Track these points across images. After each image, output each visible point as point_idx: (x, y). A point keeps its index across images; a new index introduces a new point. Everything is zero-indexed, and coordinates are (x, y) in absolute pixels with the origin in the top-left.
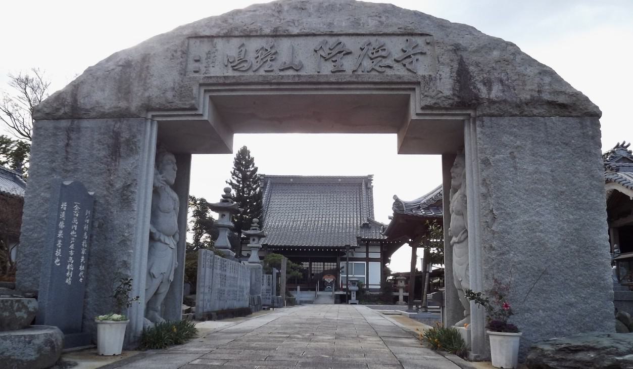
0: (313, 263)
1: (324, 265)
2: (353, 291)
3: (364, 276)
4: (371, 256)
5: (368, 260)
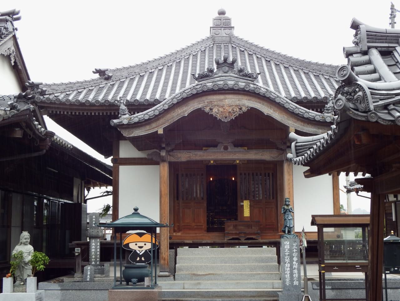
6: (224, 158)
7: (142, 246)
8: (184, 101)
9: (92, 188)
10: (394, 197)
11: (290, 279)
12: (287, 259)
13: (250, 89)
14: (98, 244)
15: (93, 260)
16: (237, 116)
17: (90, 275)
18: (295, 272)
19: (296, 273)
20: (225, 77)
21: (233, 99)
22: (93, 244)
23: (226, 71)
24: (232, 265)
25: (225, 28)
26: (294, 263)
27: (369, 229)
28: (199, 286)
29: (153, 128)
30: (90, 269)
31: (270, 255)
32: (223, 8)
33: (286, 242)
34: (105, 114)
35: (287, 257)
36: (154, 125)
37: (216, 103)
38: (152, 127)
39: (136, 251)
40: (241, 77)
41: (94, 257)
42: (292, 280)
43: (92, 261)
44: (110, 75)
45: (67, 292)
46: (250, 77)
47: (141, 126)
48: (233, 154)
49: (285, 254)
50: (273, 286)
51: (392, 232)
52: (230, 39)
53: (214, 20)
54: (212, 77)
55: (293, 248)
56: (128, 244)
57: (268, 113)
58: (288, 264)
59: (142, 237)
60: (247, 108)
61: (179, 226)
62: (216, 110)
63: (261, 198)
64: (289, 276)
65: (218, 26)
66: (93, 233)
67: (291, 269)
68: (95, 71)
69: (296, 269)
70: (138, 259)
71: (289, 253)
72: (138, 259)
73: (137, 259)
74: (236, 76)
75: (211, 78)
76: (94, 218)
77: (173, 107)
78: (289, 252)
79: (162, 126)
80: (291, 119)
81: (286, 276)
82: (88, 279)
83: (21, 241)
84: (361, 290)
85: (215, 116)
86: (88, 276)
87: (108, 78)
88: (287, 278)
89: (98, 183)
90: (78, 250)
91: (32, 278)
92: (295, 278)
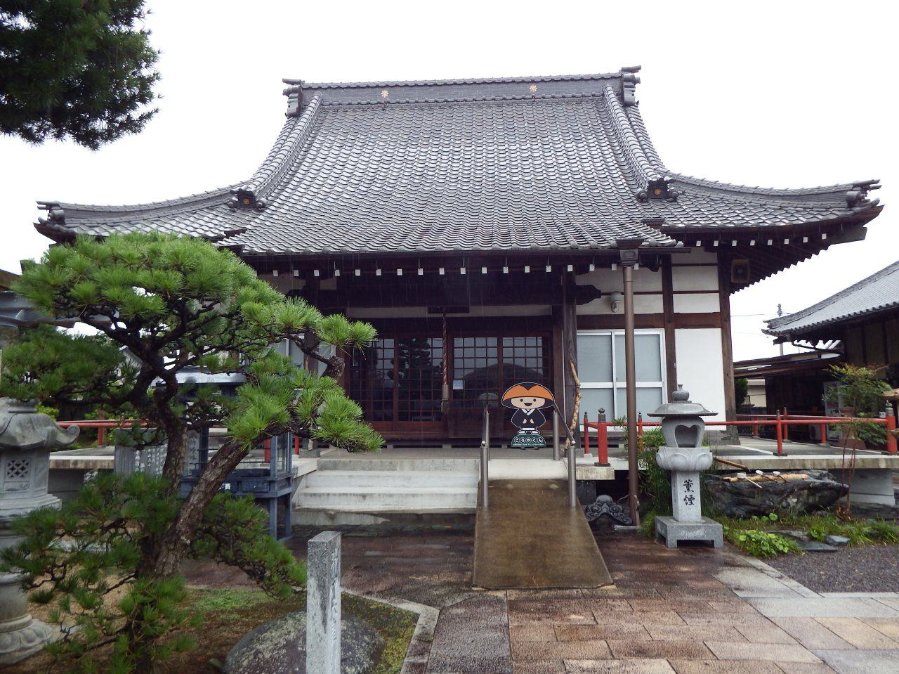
0: (458, 342)
1: (500, 346)
2: (687, 472)
3: (659, 384)
4: (683, 305)
5: (672, 321)
61: (264, 345)
63: (746, 261)
70: (525, 421)
72: (525, 421)
84: (471, 349)
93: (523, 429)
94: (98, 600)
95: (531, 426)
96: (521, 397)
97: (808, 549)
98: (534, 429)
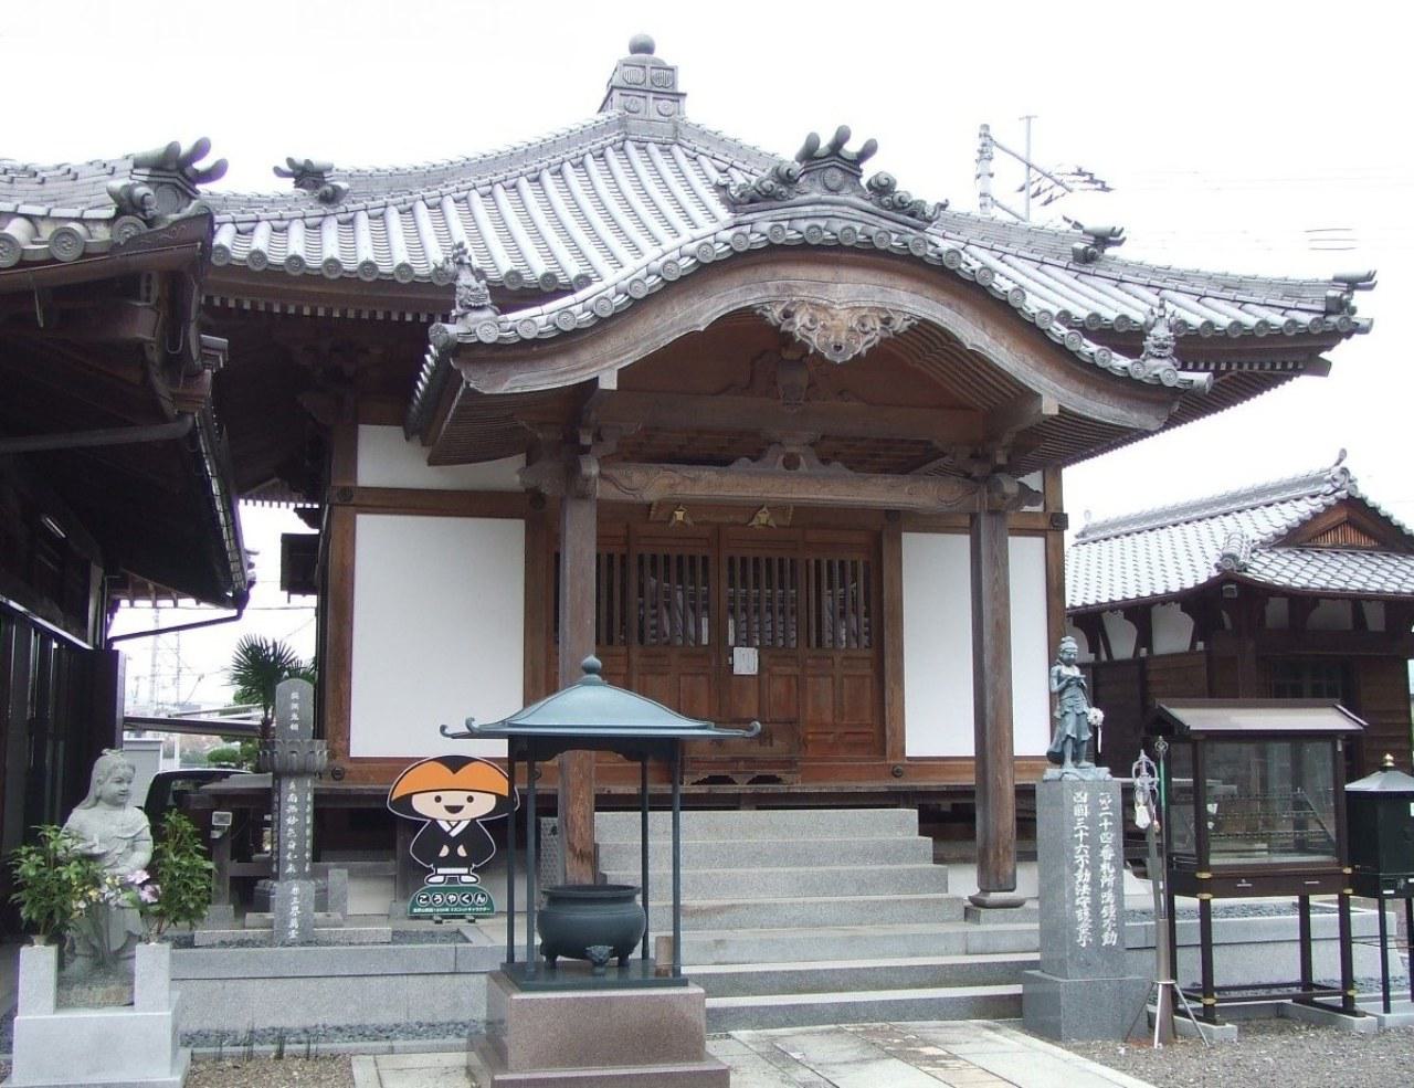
6: (789, 495)
7: (460, 804)
8: (674, 287)
9: (124, 603)
10: (1090, 652)
11: (1091, 924)
12: (1082, 853)
13: (926, 255)
14: (309, 798)
15: (289, 857)
16: (874, 346)
17: (298, 916)
18: (1108, 900)
19: (1108, 904)
20: (828, 207)
21: (863, 286)
22: (293, 798)
23: (832, 185)
24: (798, 872)
25: (659, 96)
26: (1104, 867)
27: (1340, 749)
28: (721, 952)
29: (584, 368)
30: (298, 896)
31: (899, 836)
32: (647, 33)
33: (1079, 794)
34: (367, 317)
35: (1082, 846)
36: (585, 356)
37: (805, 293)
38: (580, 365)
39: (439, 822)
40: (884, 212)
41: (292, 846)
42: (1097, 930)
43: (287, 863)
44: (344, 185)
45: (224, 987)
46: (912, 215)
47: (540, 357)
48: (819, 482)
49: (1076, 836)
50: (967, 945)
51: (1389, 757)
52: (676, 129)
53: (625, 65)
54: (789, 202)
55: (1101, 815)
56: (408, 797)
57: (975, 342)
58: (1084, 871)
59: (459, 773)
60: (908, 320)
62: (806, 319)
64: (1086, 914)
65: (638, 87)
66: (294, 755)
67: (1096, 890)
68: (285, 167)
69: (1110, 890)
71: (1087, 834)
72: (445, 851)
73: (465, 848)
74: (869, 205)
75: (784, 204)
76: (295, 701)
77: (637, 306)
78: (1087, 828)
79: (616, 364)
80: (1047, 369)
81: (1079, 912)
82: (293, 934)
83: (95, 789)
85: (801, 341)
86: (294, 923)
87: (331, 198)
88: (1081, 922)
89: (151, 586)
90: (221, 819)
91: (155, 948)
92: (1108, 921)
93: (440, 871)
94: (1055, 921)
95: (458, 862)
96: (437, 792)
97: (396, 1067)
98: (465, 870)
